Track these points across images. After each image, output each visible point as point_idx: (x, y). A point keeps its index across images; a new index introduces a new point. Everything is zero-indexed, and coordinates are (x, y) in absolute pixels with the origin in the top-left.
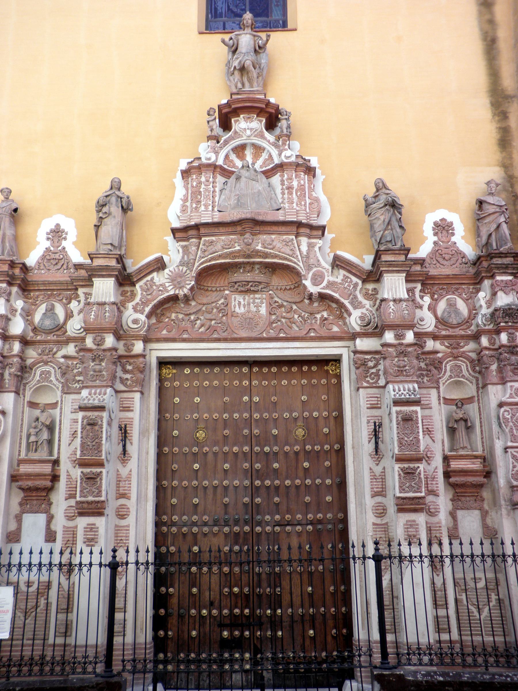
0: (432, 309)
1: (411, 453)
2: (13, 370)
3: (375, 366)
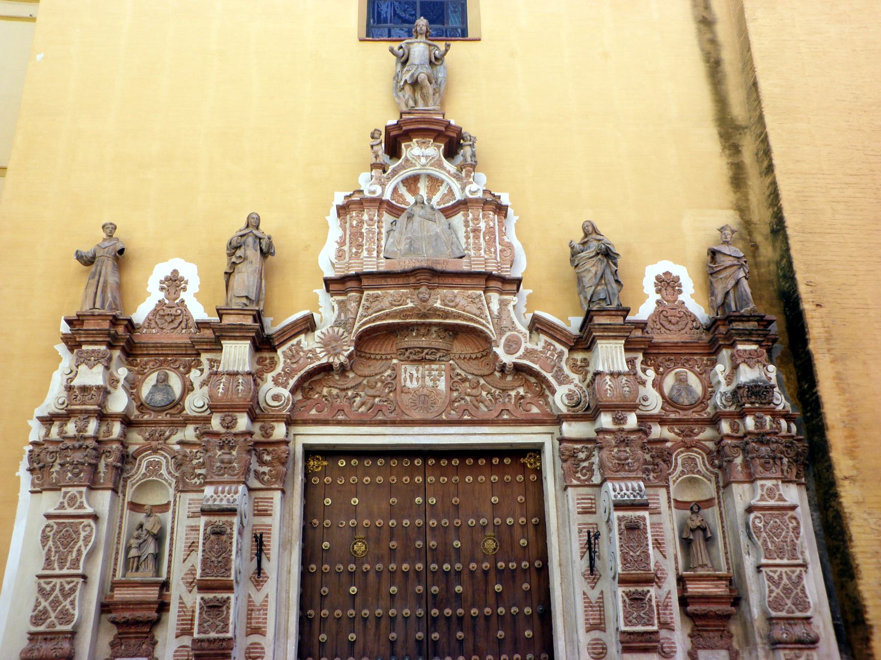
0: (658, 385)
1: (639, 572)
3: (588, 458)
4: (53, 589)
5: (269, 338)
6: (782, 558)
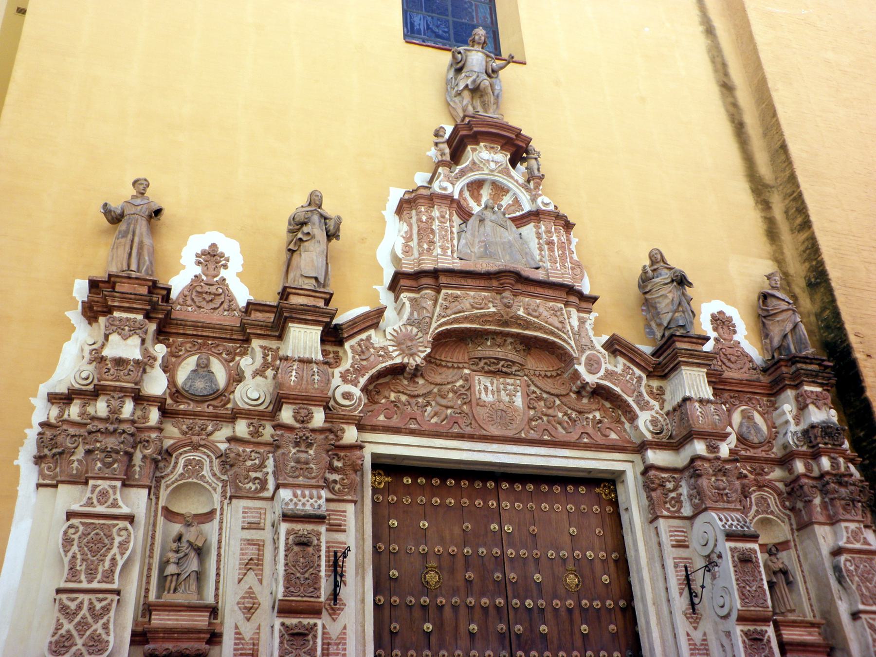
1: (758, 609)
2: (148, 452)
3: (675, 489)
4: (80, 607)
5: (338, 327)
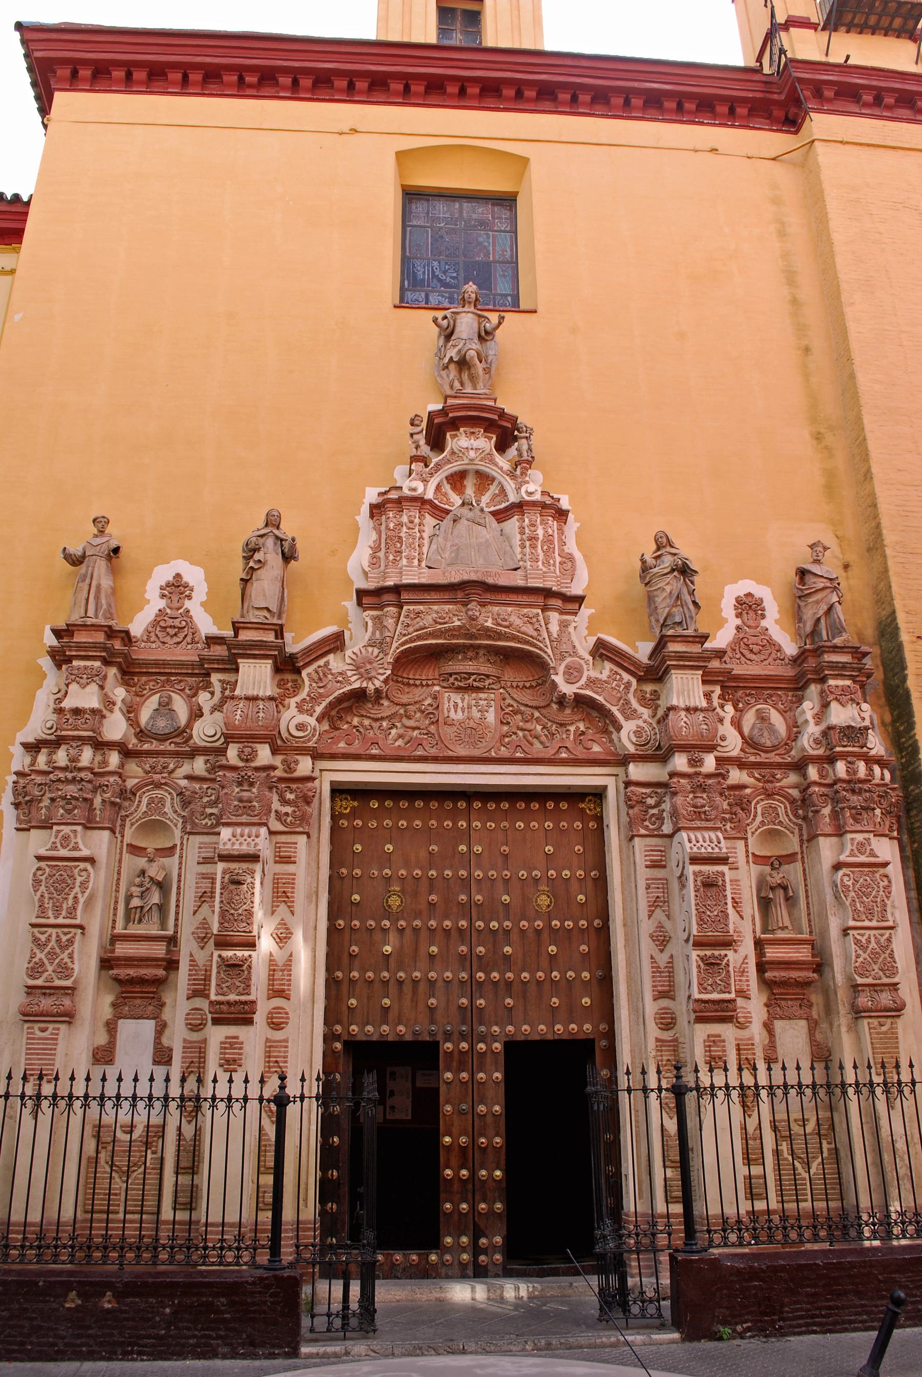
0: (737, 724)
3: (657, 805)
5: (292, 657)
6: (870, 920)
